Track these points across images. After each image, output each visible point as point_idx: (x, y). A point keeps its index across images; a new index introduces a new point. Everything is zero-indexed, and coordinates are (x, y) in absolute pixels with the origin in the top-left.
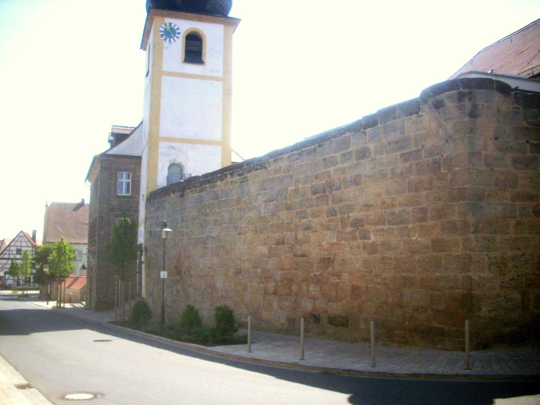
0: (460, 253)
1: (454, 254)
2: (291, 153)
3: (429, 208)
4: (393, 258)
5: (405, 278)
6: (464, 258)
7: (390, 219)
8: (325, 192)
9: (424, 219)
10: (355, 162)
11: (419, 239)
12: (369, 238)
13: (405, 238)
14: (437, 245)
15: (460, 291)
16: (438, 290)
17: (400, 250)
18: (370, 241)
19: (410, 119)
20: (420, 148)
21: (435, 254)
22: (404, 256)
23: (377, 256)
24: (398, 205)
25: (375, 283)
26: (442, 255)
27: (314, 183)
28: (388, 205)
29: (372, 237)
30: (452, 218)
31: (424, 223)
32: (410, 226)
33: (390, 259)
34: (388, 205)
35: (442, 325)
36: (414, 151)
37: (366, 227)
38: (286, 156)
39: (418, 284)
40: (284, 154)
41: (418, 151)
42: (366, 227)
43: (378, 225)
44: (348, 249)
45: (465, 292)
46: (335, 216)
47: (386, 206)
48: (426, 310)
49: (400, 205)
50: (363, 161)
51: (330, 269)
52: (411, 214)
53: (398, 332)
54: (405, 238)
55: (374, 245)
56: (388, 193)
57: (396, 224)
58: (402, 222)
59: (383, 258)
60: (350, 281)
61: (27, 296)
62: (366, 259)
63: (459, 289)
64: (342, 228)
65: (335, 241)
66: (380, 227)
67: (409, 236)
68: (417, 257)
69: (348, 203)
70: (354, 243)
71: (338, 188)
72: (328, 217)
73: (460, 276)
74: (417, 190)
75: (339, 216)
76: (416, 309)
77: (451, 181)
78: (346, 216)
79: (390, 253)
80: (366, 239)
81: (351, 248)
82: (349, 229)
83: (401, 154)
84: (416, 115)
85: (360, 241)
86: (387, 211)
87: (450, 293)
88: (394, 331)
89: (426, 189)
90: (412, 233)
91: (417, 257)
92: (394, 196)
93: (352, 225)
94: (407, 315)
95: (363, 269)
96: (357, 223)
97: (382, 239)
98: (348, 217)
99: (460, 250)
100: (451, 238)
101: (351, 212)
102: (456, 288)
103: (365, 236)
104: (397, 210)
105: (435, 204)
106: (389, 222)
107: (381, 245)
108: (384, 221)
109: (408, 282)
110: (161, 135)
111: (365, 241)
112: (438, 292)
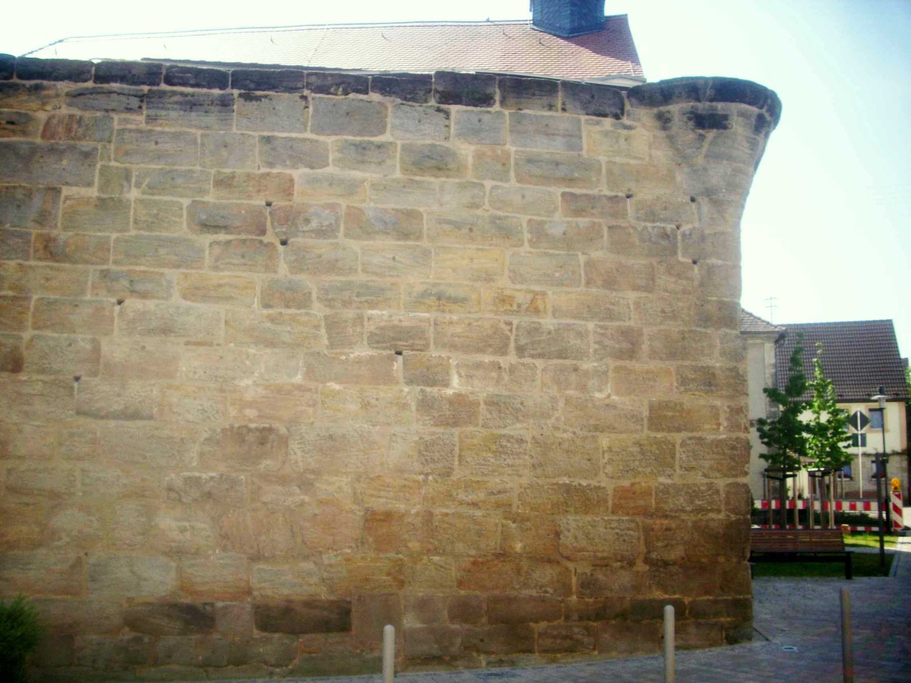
0: (724, 436)
1: (710, 437)
2: (90, 84)
3: (646, 331)
4: (528, 438)
5: (568, 489)
6: (733, 448)
7: (523, 341)
8: (263, 232)
9: (632, 354)
10: (398, 174)
11: (615, 397)
12: (447, 385)
13: (570, 392)
14: (660, 417)
15: (721, 516)
16: (666, 517)
17: (553, 420)
18: (449, 392)
19: (598, 123)
20: (620, 194)
21: (659, 435)
22: (565, 435)
23: (475, 432)
24: (550, 310)
25: (461, 503)
26: (678, 437)
27: (210, 198)
28: (519, 306)
29: (455, 381)
30: (706, 361)
31: (627, 363)
32: (587, 365)
33: (521, 441)
34: (519, 306)
35: (674, 593)
36: (605, 196)
37: (434, 353)
38: (64, 86)
39: (610, 504)
40: (57, 79)
41: (614, 199)
42: (434, 353)
43: (480, 350)
44: (353, 407)
45: (733, 517)
46: (305, 307)
47: (515, 307)
48: (631, 564)
49: (556, 312)
50: (432, 179)
51: (266, 464)
52: (591, 338)
53: (543, 625)
54: (570, 392)
55: (458, 400)
56: (516, 277)
57: (541, 356)
58: (562, 354)
59: (496, 439)
60: (357, 501)
61: (417, 182)
62: (427, 438)
63: (719, 511)
64: (332, 346)
65: (298, 379)
66: (487, 359)
67: (583, 388)
68: (604, 441)
69: (361, 278)
70: (386, 393)
71: (321, 233)
72: (267, 306)
73: (721, 483)
74: (610, 283)
75: (318, 310)
76: (602, 564)
77: (702, 285)
78: (349, 314)
79: (518, 425)
80: (428, 385)
81: (366, 405)
82: (362, 351)
83: (564, 194)
84: (614, 120)
85: (406, 389)
86: (515, 322)
87: (695, 523)
88: (532, 624)
89: (636, 288)
90: (592, 383)
91: (604, 441)
92: (537, 288)
93: (375, 340)
94: (574, 579)
95: (417, 466)
96: (396, 342)
97: (491, 390)
98: (359, 319)
99: (721, 428)
100: (702, 402)
101: (373, 305)
102: (712, 510)
103: (431, 376)
104: (548, 322)
105: (661, 324)
106: (521, 350)
107: (486, 403)
108: (506, 345)
109: (583, 499)
110: (905, 457)
111: (428, 389)
112: (666, 522)
